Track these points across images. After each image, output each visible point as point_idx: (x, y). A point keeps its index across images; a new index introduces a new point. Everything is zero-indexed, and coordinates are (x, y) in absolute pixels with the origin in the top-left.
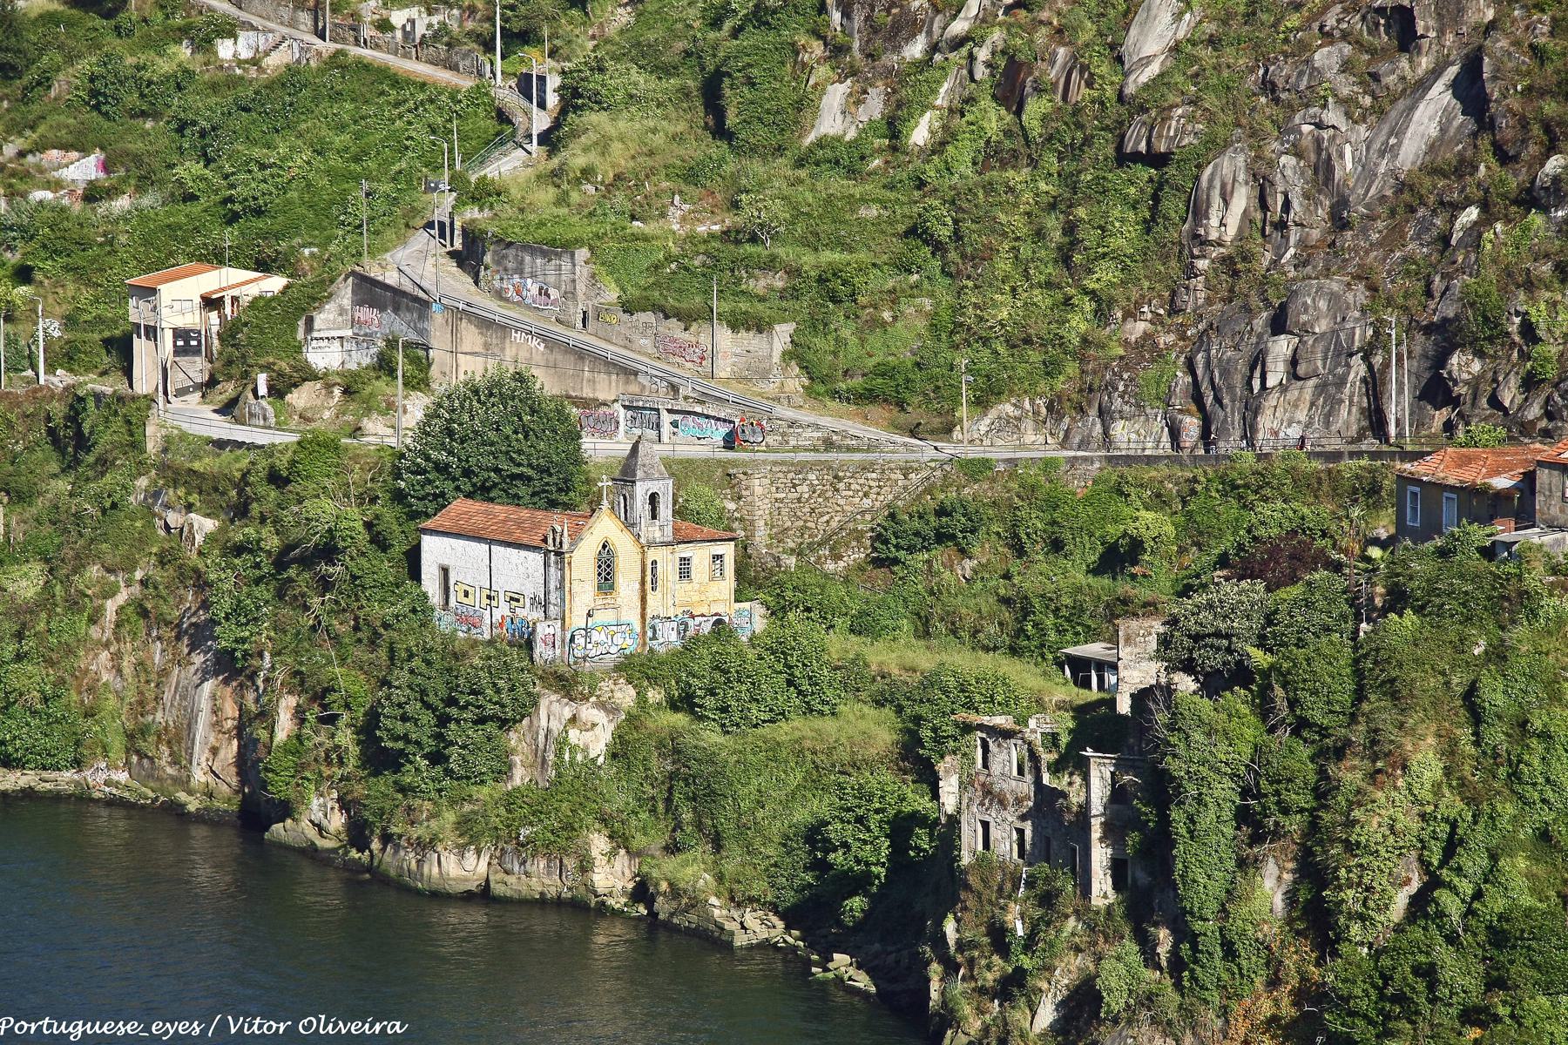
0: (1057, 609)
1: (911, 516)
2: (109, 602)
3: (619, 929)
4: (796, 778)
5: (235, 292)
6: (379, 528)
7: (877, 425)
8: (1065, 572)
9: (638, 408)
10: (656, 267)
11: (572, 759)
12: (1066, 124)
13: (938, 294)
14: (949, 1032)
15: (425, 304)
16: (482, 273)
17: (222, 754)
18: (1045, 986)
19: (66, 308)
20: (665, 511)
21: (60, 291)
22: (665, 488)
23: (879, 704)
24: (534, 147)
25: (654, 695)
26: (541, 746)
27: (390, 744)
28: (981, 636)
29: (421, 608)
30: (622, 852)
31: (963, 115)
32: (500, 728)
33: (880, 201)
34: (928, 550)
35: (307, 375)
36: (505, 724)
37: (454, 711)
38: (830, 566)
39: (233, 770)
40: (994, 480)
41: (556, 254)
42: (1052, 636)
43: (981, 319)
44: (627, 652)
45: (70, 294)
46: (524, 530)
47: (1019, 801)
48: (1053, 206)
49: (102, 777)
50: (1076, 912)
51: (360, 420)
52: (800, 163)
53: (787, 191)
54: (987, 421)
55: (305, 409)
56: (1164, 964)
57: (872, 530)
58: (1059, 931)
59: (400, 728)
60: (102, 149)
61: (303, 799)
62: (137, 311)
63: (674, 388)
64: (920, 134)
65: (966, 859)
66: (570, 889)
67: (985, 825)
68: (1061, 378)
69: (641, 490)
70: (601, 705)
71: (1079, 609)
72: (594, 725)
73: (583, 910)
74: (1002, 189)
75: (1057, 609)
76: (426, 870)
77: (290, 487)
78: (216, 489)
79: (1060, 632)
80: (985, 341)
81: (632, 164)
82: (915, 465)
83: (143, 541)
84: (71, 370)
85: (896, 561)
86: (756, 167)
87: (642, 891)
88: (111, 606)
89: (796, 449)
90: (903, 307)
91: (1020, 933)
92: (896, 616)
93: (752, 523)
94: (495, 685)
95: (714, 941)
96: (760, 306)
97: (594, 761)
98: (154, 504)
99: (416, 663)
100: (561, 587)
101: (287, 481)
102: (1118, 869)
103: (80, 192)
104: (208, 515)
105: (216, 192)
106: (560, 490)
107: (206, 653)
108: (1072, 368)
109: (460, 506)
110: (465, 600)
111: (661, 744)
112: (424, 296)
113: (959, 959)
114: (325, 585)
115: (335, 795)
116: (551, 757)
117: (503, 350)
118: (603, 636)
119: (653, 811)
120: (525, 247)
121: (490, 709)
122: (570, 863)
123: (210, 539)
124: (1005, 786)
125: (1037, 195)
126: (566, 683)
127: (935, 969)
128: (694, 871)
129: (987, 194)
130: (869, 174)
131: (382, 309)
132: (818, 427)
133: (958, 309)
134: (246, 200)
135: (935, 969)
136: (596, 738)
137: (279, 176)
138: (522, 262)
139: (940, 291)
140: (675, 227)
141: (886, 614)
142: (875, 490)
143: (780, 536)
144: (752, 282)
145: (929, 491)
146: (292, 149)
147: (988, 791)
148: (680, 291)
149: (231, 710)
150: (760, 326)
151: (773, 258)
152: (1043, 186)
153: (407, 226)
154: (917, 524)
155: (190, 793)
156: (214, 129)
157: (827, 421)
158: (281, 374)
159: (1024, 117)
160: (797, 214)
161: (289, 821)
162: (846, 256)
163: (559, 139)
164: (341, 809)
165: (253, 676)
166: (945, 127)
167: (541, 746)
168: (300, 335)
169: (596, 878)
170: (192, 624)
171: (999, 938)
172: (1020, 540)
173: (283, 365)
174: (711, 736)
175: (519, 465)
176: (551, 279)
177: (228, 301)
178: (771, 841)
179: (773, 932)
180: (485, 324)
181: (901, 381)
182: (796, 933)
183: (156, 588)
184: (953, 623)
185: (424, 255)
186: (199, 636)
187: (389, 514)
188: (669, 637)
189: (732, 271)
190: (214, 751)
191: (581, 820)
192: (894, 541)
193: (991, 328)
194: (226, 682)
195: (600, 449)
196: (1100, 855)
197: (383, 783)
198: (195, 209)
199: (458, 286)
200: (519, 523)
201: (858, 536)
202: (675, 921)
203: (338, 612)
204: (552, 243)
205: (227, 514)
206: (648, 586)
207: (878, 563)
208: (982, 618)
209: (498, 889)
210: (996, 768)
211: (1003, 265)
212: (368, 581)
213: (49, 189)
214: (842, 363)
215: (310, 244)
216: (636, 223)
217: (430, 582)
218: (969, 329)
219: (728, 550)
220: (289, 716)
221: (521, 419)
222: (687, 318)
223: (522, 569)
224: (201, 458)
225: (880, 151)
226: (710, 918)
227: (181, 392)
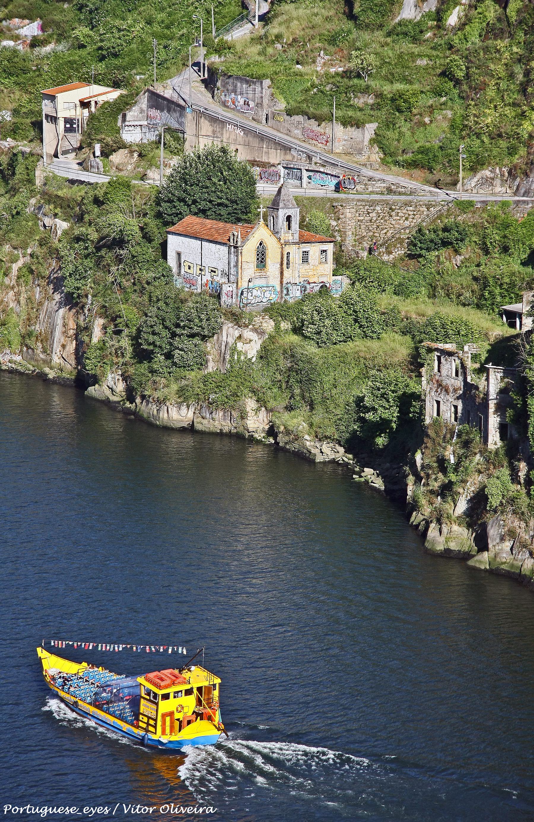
0: (502, 284)
1: (430, 231)
2: (14, 265)
3: (260, 448)
4: (354, 373)
5: (95, 99)
6: (147, 230)
7: (417, 180)
8: (508, 263)
9: (291, 168)
10: (306, 91)
11: (239, 358)
12: (529, 14)
13: (455, 108)
14: (414, 513)
15: (183, 108)
16: (216, 92)
17: (67, 348)
18: (461, 491)
19: (15, 105)
20: (295, 225)
21: (12, 95)
22: (295, 213)
23: (404, 333)
24: (256, 22)
25: (285, 325)
26: (223, 351)
27: (145, 347)
28: (462, 298)
29: (167, 274)
30: (263, 409)
31: (476, 9)
32: (202, 340)
33: (428, 56)
34: (438, 250)
35: (122, 145)
36: (204, 338)
37: (178, 331)
38: (385, 258)
39: (73, 357)
40: (474, 212)
41: (253, 82)
42: (499, 299)
43: (477, 123)
44: (272, 301)
45: (17, 97)
46: (219, 234)
47: (455, 390)
48: (519, 61)
49: (7, 358)
50: (480, 451)
51: (146, 171)
52: (389, 34)
53: (379, 50)
54: (476, 179)
55: (119, 164)
56: (522, 481)
57: (408, 238)
58: (471, 462)
59: (151, 338)
60: (41, 18)
61: (104, 374)
62: (47, 107)
63: (309, 158)
64: (453, 19)
65: (428, 421)
66: (235, 428)
67: (438, 403)
68: (517, 156)
69: (282, 214)
70: (255, 330)
71: (512, 285)
72: (251, 341)
73: (242, 439)
74: (493, 51)
75: (502, 284)
76: (161, 415)
77: (104, 207)
78: (69, 206)
79: (503, 297)
80: (478, 135)
81: (302, 33)
82: (433, 203)
83: (32, 232)
84: (15, 139)
85: (420, 256)
86: (366, 36)
87: (272, 432)
88: (15, 267)
89: (372, 192)
90: (436, 115)
91: (452, 461)
92: (419, 285)
93: (345, 232)
94: (199, 317)
95: (304, 458)
96: (359, 114)
97: (250, 360)
98: (38, 213)
99: (161, 304)
100: (236, 266)
101: (103, 203)
102: (503, 428)
103: (28, 42)
104: (64, 220)
105: (95, 43)
106: (243, 212)
107: (61, 294)
108: (523, 151)
109: (189, 219)
110: (189, 271)
111: (285, 352)
112: (182, 103)
113: (422, 474)
114: (119, 260)
115: (120, 373)
116: (228, 357)
117: (222, 134)
118: (259, 292)
119: (280, 387)
120: (238, 78)
121: (196, 330)
122: (235, 414)
123: (65, 233)
124: (448, 382)
125: (512, 54)
126: (236, 317)
127: (411, 479)
128: (297, 422)
129: (485, 54)
130: (424, 41)
131: (162, 110)
132: (384, 181)
133: (465, 117)
134: (109, 48)
135: (411, 479)
136: (252, 349)
137: (127, 35)
138: (236, 86)
139: (456, 107)
140: (319, 69)
141: (413, 284)
142: (412, 216)
143: (360, 240)
144: (356, 100)
145: (440, 217)
146: (135, 21)
147: (440, 385)
148: (318, 104)
149: (72, 325)
150: (358, 124)
151: (368, 87)
152: (515, 49)
153: (184, 64)
154: (433, 236)
155: (51, 368)
156: (96, 9)
157: (391, 178)
158: (107, 145)
159: (508, 10)
160: (384, 63)
161: (97, 386)
162: (408, 87)
163: (269, 19)
164: (123, 380)
165: (83, 308)
166: (466, 16)
167: (223, 351)
168: (119, 124)
169: (248, 422)
170: (54, 278)
171: (442, 464)
172: (487, 246)
173: (109, 139)
174: (311, 349)
175: (221, 198)
176: (250, 96)
177: (93, 104)
178: (339, 406)
179: (337, 455)
180: (214, 120)
181: (431, 157)
182: (351, 456)
183: (37, 258)
184: (448, 291)
185: (188, 81)
186: (58, 284)
187: (153, 224)
188: (296, 294)
189: (346, 93)
190: (64, 346)
191: (242, 391)
192: (419, 245)
193: (482, 128)
194: (70, 309)
195: (265, 189)
196: (494, 421)
197: (144, 367)
198: (83, 52)
199: (203, 98)
200: (217, 231)
201: (401, 241)
202: (288, 447)
203: (125, 275)
204: (252, 76)
205: (74, 220)
206: (285, 266)
207: (411, 257)
208: (463, 288)
209: (198, 427)
210: (444, 372)
211: (491, 92)
212: (140, 259)
213: (12, 40)
214: (401, 147)
215: (141, 74)
216: (299, 66)
217: (172, 261)
218: (471, 128)
219: (330, 248)
220: (99, 329)
221: (222, 173)
222: (319, 119)
223: (217, 255)
224: (62, 189)
225: (431, 28)
226: (304, 447)
227: (65, 153)
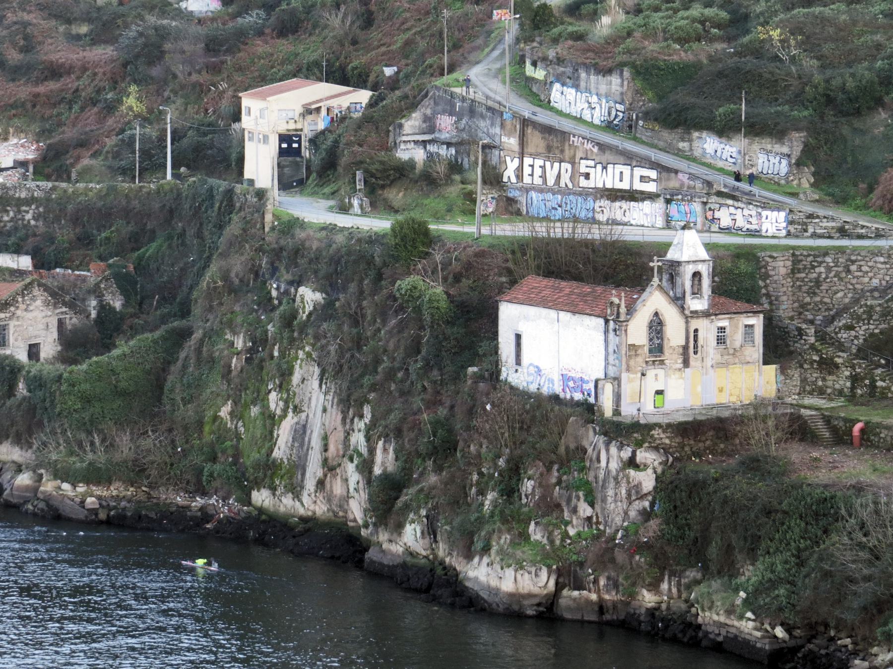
5: (330, 103)
206: (691, 350)
